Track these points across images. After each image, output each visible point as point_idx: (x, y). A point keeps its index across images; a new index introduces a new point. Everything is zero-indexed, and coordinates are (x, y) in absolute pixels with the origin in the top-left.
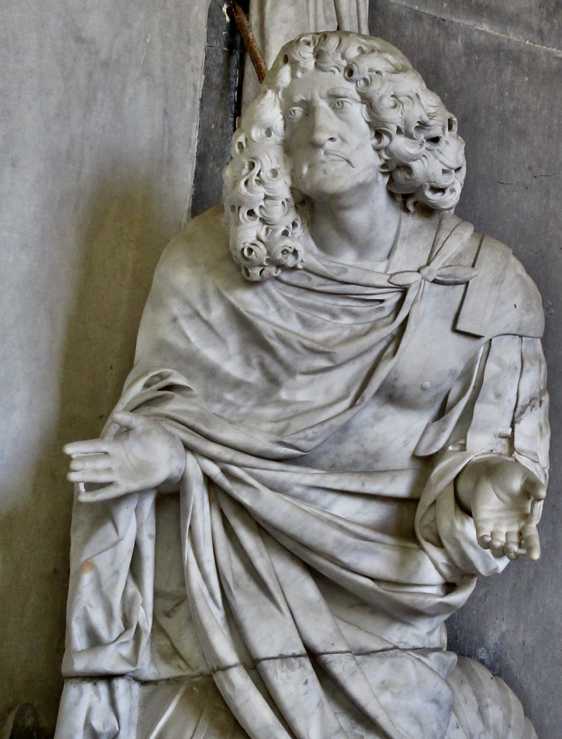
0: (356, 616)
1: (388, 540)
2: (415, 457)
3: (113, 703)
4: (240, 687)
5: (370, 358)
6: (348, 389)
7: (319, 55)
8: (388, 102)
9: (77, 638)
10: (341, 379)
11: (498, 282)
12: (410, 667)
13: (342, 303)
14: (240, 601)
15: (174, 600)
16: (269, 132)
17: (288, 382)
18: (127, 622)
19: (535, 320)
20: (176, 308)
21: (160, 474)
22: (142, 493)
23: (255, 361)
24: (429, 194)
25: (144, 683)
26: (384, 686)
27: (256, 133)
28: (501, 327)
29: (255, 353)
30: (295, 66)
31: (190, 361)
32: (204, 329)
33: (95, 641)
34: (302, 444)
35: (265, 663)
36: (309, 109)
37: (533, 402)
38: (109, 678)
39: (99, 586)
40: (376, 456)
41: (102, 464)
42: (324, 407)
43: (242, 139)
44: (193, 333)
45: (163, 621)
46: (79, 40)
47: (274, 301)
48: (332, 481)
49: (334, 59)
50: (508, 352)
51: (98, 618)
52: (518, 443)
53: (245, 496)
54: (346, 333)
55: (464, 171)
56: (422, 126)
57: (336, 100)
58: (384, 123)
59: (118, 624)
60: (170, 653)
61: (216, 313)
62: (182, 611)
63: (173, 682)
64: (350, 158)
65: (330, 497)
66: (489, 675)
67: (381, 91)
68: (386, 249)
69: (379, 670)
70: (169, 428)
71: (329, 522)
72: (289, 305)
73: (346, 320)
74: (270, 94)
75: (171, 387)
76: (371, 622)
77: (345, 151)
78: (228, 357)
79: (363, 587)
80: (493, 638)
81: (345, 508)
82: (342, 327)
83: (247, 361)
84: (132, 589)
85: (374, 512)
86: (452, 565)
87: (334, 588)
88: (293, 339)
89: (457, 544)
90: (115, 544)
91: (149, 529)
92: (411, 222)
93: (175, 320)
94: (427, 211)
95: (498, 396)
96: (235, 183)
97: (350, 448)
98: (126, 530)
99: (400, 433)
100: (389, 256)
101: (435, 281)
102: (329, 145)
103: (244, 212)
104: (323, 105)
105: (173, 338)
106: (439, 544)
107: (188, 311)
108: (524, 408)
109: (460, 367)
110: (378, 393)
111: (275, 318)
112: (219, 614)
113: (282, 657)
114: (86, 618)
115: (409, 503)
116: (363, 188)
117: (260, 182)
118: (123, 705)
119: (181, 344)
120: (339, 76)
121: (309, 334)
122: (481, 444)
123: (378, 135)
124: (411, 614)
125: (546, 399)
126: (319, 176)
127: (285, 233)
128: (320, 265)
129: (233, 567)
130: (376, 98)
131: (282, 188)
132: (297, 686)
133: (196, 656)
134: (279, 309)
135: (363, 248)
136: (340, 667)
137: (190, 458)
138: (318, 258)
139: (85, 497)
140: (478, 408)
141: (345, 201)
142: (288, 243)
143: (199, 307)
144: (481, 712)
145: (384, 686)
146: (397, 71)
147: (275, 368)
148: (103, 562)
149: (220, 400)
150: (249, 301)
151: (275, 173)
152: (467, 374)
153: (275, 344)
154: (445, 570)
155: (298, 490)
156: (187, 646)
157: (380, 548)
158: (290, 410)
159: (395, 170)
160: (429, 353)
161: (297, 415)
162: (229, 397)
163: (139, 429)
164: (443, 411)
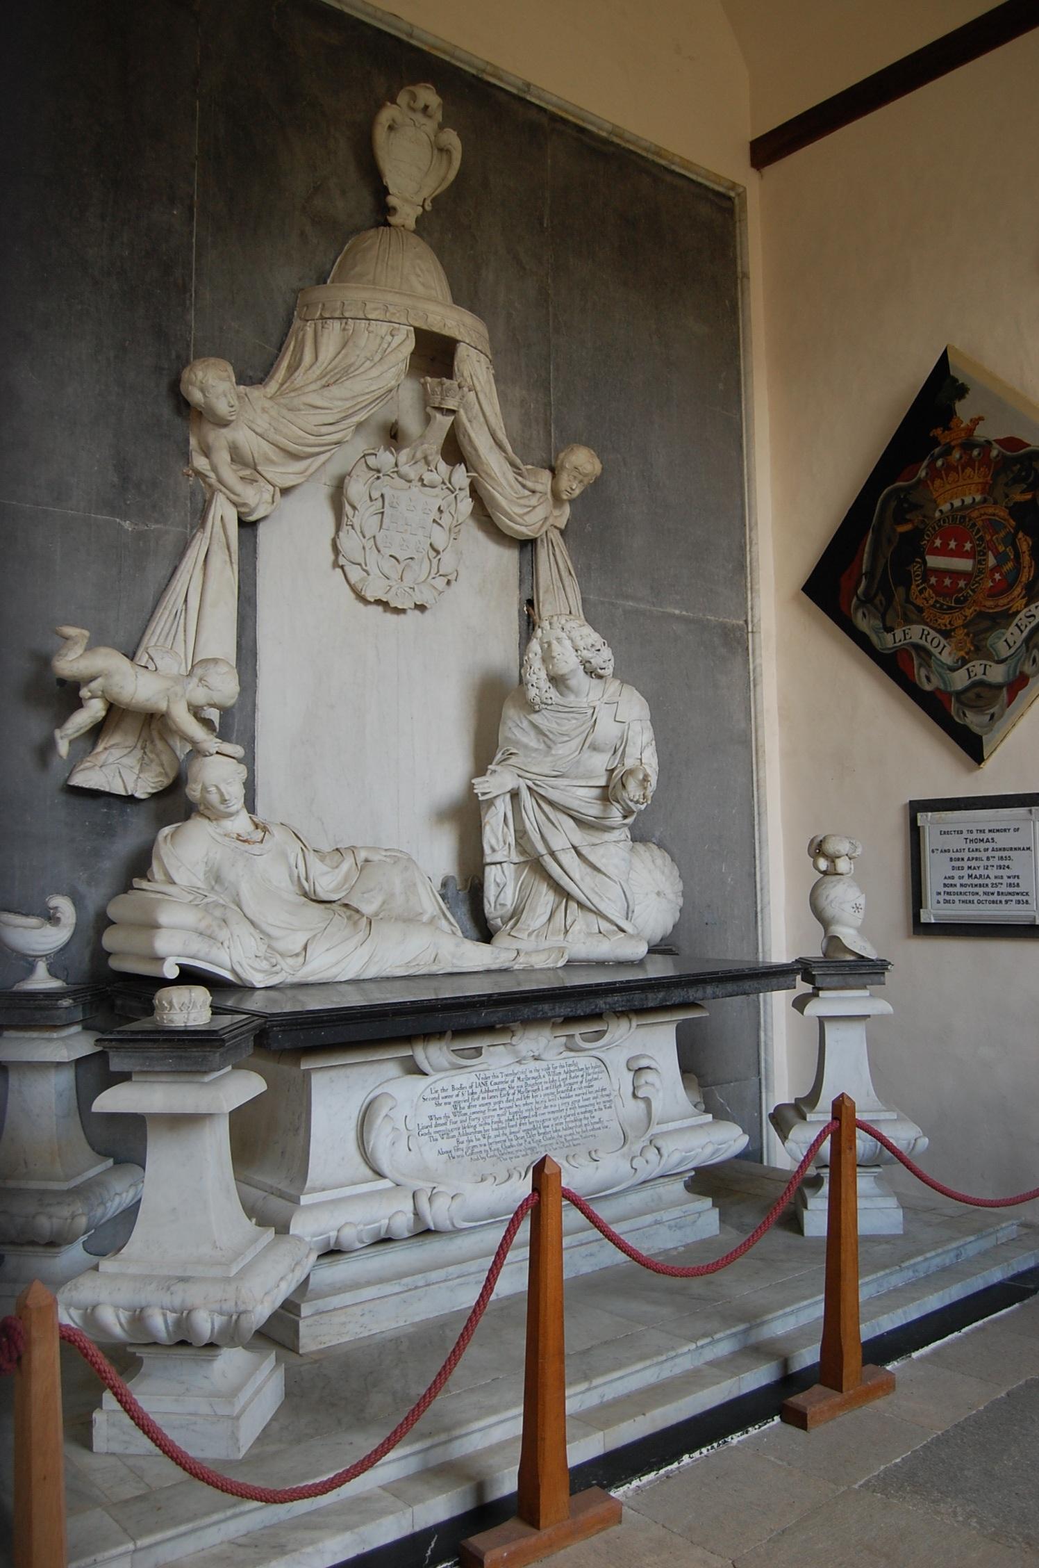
0: (591, 832)
4: (548, 860)
9: (487, 850)
10: (577, 742)
12: (612, 848)
14: (544, 831)
15: (521, 834)
19: (646, 714)
20: (510, 724)
29: (541, 737)
31: (517, 743)
33: (494, 850)
37: (647, 745)
41: (486, 785)
44: (516, 731)
49: (556, 625)
50: (636, 727)
51: (493, 842)
61: (525, 724)
64: (567, 661)
67: (575, 634)
78: (531, 740)
81: (582, 792)
85: (596, 792)
87: (580, 822)
91: (509, 807)
92: (595, 681)
94: (600, 677)
99: (599, 763)
104: (554, 642)
112: (539, 836)
115: (606, 787)
120: (559, 630)
122: (630, 763)
124: (610, 829)
129: (541, 818)
131: (543, 675)
132: (570, 860)
135: (577, 694)
136: (584, 851)
139: (481, 798)
142: (548, 695)
145: (603, 856)
147: (549, 742)
148: (493, 821)
150: (535, 718)
152: (622, 738)
156: (528, 849)
159: (585, 663)
160: (607, 730)
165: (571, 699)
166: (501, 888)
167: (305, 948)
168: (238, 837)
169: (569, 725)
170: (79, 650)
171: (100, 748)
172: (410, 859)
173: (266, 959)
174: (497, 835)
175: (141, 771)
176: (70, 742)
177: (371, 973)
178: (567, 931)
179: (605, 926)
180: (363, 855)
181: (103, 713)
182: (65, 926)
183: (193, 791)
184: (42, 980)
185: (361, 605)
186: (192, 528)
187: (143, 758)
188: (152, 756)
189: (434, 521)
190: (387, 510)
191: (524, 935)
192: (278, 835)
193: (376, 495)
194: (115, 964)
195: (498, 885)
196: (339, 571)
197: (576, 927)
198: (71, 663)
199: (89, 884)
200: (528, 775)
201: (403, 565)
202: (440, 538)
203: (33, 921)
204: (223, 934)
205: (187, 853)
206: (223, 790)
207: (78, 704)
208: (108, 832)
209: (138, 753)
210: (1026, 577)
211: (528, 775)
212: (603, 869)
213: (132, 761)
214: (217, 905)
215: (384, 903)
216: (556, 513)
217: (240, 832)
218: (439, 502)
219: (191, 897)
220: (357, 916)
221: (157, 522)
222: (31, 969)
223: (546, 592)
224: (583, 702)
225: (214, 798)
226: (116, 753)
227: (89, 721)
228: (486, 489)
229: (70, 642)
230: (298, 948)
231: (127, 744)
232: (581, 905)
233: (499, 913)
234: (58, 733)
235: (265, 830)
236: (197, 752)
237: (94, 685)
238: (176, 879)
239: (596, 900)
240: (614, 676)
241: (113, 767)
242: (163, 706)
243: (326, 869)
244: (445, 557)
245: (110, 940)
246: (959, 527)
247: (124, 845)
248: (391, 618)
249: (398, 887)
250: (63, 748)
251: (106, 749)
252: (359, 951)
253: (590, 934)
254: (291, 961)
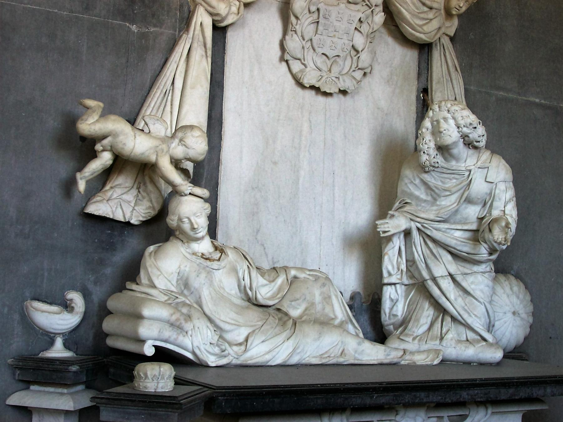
1: (471, 242)
2: (478, 218)
3: (396, 291)
5: (462, 191)
6: (456, 200)
7: (439, 107)
8: (460, 118)
9: (385, 274)
10: (454, 198)
11: (498, 167)
12: (480, 277)
13: (453, 176)
14: (429, 262)
16: (427, 129)
17: (439, 200)
18: (398, 269)
19: (510, 177)
20: (406, 181)
21: (403, 227)
22: (400, 233)
23: (429, 194)
24: (475, 143)
25: (406, 285)
26: (472, 283)
27: (424, 130)
28: (499, 179)
29: (429, 191)
30: (433, 110)
31: (411, 195)
32: (415, 186)
33: (390, 274)
34: (443, 216)
35: (437, 278)
36: (438, 122)
37: (510, 201)
38: (395, 284)
39: (390, 259)
40: (466, 219)
41: (386, 226)
42: (452, 205)
43: (420, 132)
44: (411, 187)
45: (409, 268)
46: (378, 108)
47: (433, 177)
48: (453, 226)
49: (444, 108)
50: (502, 186)
51: (390, 268)
52: (506, 212)
53: (429, 233)
54: (455, 184)
55: (486, 136)
56: (471, 124)
57: (445, 119)
58: (460, 124)
59: (396, 270)
60: (412, 277)
61: (417, 181)
62: (414, 266)
63: (413, 285)
64: (451, 134)
65: (453, 231)
66: (514, 278)
67: (458, 115)
68: (464, 160)
69: (471, 279)
70: (405, 215)
71: (453, 238)
72: (438, 178)
73: (454, 181)
74: (427, 119)
75: (406, 203)
76: (468, 266)
77: (449, 133)
78: (421, 193)
79: (464, 256)
80: (515, 267)
81: (458, 234)
82: (454, 183)
83: (427, 194)
84: (399, 259)
85: (468, 235)
86: (490, 248)
87: (456, 256)
88: (439, 187)
89: (490, 242)
90: (393, 248)
91: (403, 243)
92: (471, 151)
93: (406, 184)
94: (475, 148)
95: (500, 199)
96: (419, 144)
97: (458, 217)
98: (396, 243)
99: (473, 212)
100: (465, 161)
102: (444, 132)
103: (422, 153)
104: (442, 121)
105: (406, 189)
106: (486, 243)
107: (409, 181)
108: (508, 202)
109: (488, 192)
110: (465, 201)
111: (433, 181)
112: (424, 265)
113: (442, 276)
114: (387, 268)
115: (476, 231)
116: (455, 143)
117: (426, 144)
118: (399, 291)
119: (409, 191)
120: (446, 112)
121: (444, 185)
122: (496, 213)
123: (458, 128)
124: (478, 263)
125: (515, 199)
126: (442, 141)
127: (434, 157)
128: (445, 166)
130: (457, 118)
131: (432, 145)
132: (447, 284)
133: (419, 277)
134: (435, 179)
136: (459, 278)
137: (412, 223)
138: (445, 163)
140: (494, 203)
141: (450, 147)
142: (435, 160)
143: (412, 180)
144: (511, 289)
145: (472, 283)
146: (462, 109)
147: (435, 196)
148: (390, 253)
149: (420, 206)
150: (426, 177)
151: (430, 140)
152: (491, 193)
153: (434, 189)
154: (488, 250)
155: (444, 230)
156: (416, 275)
157: (468, 245)
158: (440, 207)
159: (464, 137)
161: (442, 209)
162: (423, 205)
163: (396, 215)
164: (485, 204)
165: (453, 164)
166: (394, 302)
167: (247, 340)
168: (203, 256)
169: (451, 183)
170: (96, 117)
171: (107, 187)
172: (327, 278)
173: (218, 345)
174: (392, 262)
175: (136, 204)
176: (87, 182)
177: (294, 360)
178: (442, 339)
179: (471, 335)
180: (293, 273)
181: (111, 162)
182: (77, 313)
183: (172, 221)
184: (58, 351)
185: (299, 90)
186: (180, 31)
187: (137, 196)
188: (144, 194)
189: (356, 28)
190: (321, 20)
191: (410, 339)
192: (231, 255)
193: (313, 9)
194: (110, 342)
195: (392, 300)
196: (284, 64)
197: (449, 336)
198: (89, 125)
199: (95, 283)
200: (418, 220)
201: (332, 60)
202: (359, 41)
203: (54, 308)
204: (188, 326)
205: (167, 266)
206: (193, 221)
207: (94, 155)
208: (110, 247)
209: (134, 192)
211: (418, 220)
212: (472, 292)
213: (130, 197)
214: (184, 304)
215: (306, 309)
216: (448, 24)
217: (205, 252)
218: (360, 15)
219: (166, 298)
220: (286, 318)
221: (155, 26)
222: (51, 343)
223: (438, 82)
224: (462, 166)
225: (186, 226)
226: (118, 191)
227: (101, 167)
228: (395, 6)
229: (90, 111)
230: (241, 339)
231: (127, 185)
232: (454, 319)
233: (392, 321)
234: (78, 175)
235: (222, 251)
236: (176, 192)
237: (106, 142)
238: (157, 283)
239: (465, 316)
240: (487, 147)
241: (116, 201)
242: (153, 158)
243: (265, 282)
244: (365, 57)
245: (108, 325)
247: (120, 257)
248: (321, 99)
249: (318, 298)
250: (82, 186)
251: (112, 188)
252: (286, 344)
253: (459, 341)
254: (235, 348)
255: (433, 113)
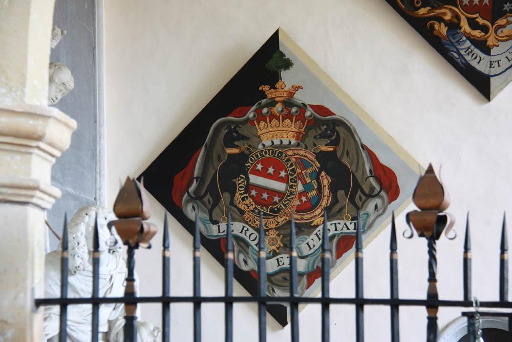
43: (74, 236)
101: (119, 273)
103: (76, 256)
210: (324, 203)
246: (275, 161)
255: (89, 218)
